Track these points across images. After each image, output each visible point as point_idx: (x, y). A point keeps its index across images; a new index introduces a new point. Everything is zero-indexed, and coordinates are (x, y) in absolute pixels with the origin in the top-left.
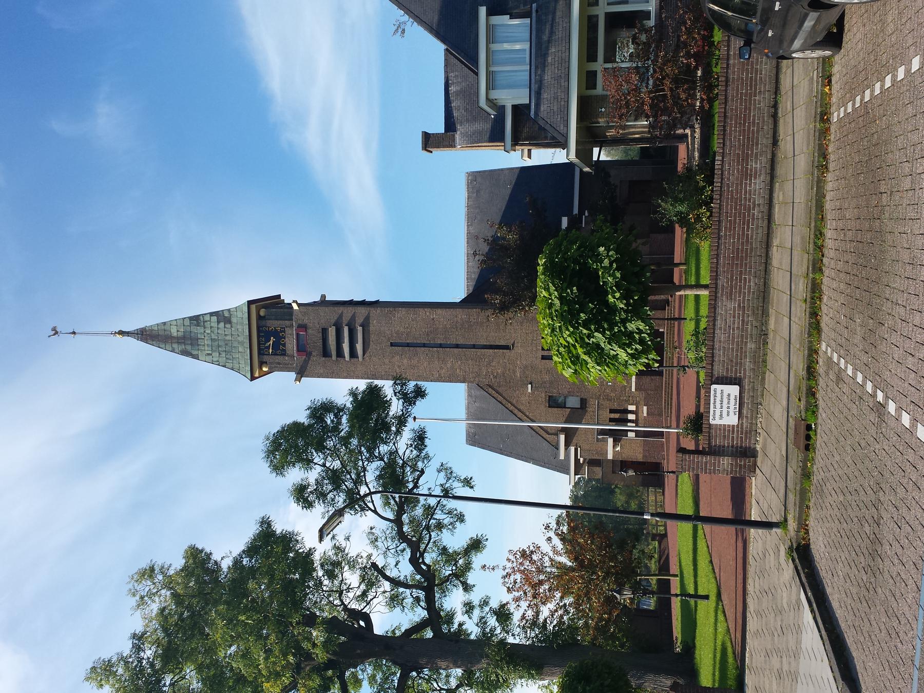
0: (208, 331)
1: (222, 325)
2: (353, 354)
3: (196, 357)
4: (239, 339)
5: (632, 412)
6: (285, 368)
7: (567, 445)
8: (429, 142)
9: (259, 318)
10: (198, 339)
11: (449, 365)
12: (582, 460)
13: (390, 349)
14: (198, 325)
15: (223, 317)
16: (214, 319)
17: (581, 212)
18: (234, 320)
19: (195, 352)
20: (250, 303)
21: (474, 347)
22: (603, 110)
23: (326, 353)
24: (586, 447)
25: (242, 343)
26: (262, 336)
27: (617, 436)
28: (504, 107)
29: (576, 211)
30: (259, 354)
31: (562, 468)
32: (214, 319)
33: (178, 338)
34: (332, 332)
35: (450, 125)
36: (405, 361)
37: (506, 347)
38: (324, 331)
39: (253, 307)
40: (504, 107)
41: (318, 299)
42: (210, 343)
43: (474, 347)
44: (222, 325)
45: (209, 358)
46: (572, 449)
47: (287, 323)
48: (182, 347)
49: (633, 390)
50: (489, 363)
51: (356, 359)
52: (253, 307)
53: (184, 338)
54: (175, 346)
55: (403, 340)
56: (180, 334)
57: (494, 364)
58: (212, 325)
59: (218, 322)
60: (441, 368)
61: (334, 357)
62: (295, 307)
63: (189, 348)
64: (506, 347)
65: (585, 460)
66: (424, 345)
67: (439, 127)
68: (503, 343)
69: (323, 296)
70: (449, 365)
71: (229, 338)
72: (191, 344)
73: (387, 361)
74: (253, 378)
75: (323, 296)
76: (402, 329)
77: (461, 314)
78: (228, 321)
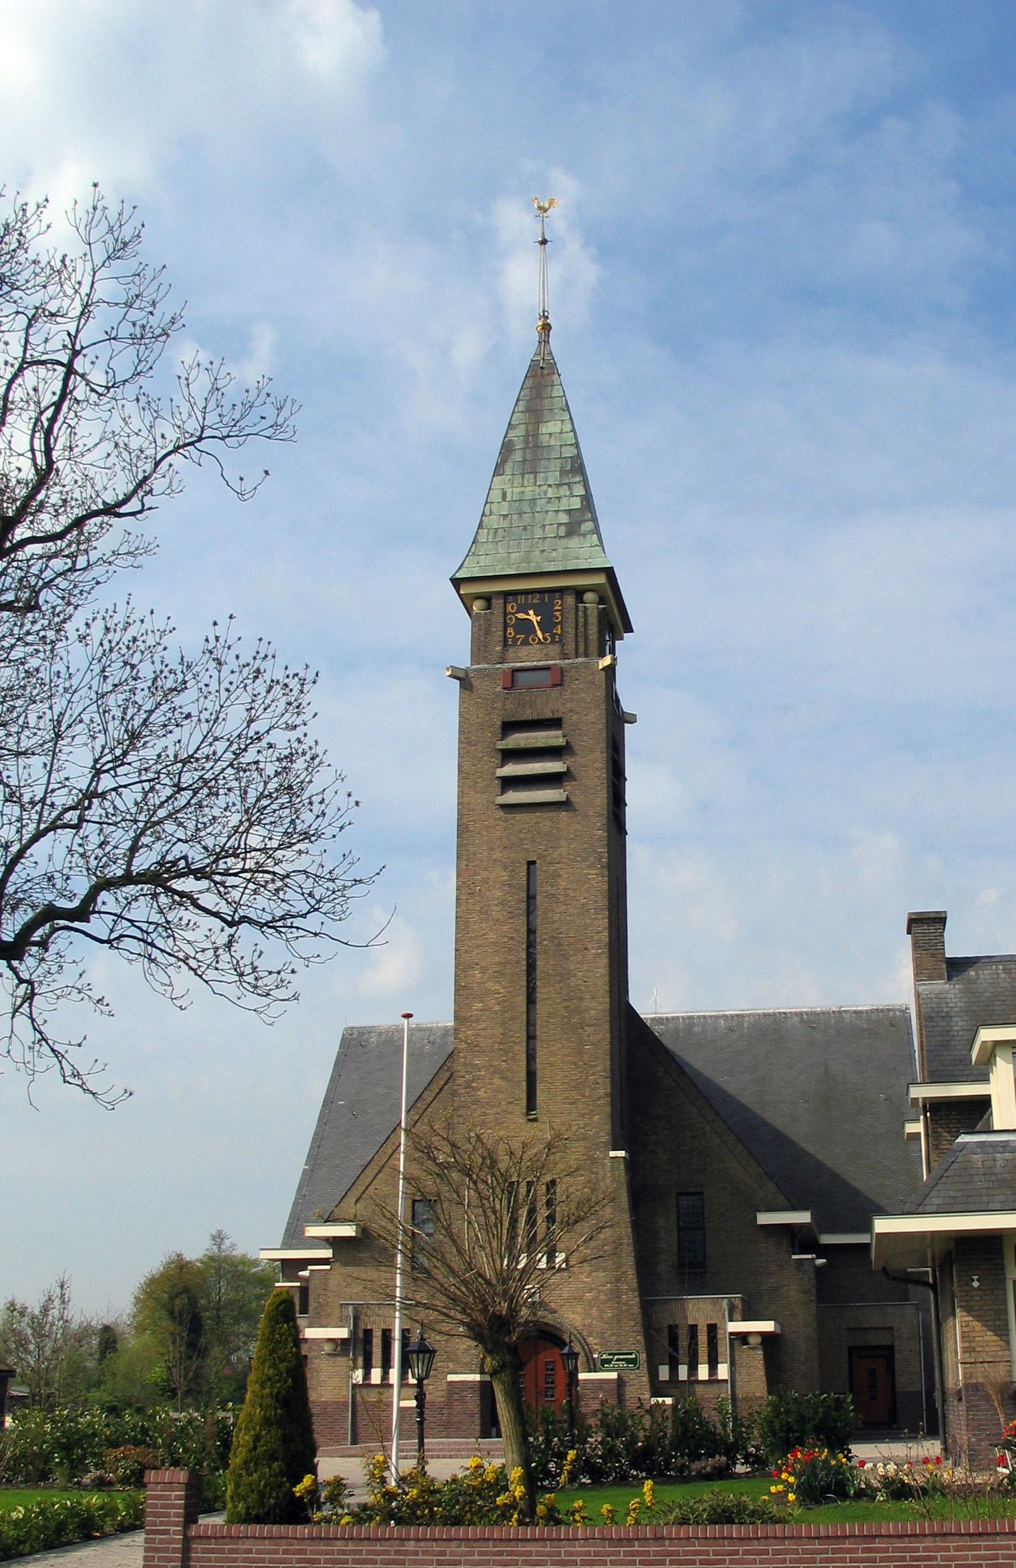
0: (551, 493)
1: (564, 518)
2: (509, 783)
3: (498, 470)
4: (537, 553)
5: (367, 1375)
6: (479, 649)
7: (334, 1242)
8: (926, 927)
9: (579, 593)
10: (535, 473)
11: (492, 986)
12: (305, 1273)
13: (522, 858)
14: (563, 473)
15: (583, 518)
16: (576, 504)
17: (823, 1250)
18: (573, 542)
19: (508, 468)
20: (609, 573)
21: (531, 1037)
22: (976, 1284)
23: (509, 727)
24: (333, 1282)
25: (527, 559)
26: (542, 600)
27: (360, 1346)
28: (986, 1080)
29: (827, 1239)
30: (506, 594)
31: (293, 1236)
32: (576, 504)
33: (536, 435)
34: (551, 738)
35: (957, 966)
36: (498, 894)
37: (531, 1105)
38: (555, 723)
39: (601, 579)
40: (986, 1080)
41: (627, 706)
42: (528, 496)
43: (531, 1037)
44: (564, 518)
45: (496, 495)
46: (327, 1253)
47: (570, 647)
48: (519, 445)
49: (451, 1378)
50: (497, 1071)
51: (499, 790)
52: (601, 579)
53: (537, 446)
54: (520, 431)
55: (543, 889)
56: (545, 440)
57: (497, 1081)
58: (564, 500)
59: (569, 512)
60: (484, 970)
61: (502, 745)
62: (607, 661)
63: (518, 456)
64: (531, 1105)
65: (306, 1280)
66: (531, 932)
67: (954, 948)
68: (540, 1097)
69: (632, 719)
70: (492, 986)
71: (538, 533)
72: (524, 461)
73: (497, 855)
74: (457, 583)
75: (632, 719)
76: (563, 883)
77: (598, 1005)
78: (572, 530)
